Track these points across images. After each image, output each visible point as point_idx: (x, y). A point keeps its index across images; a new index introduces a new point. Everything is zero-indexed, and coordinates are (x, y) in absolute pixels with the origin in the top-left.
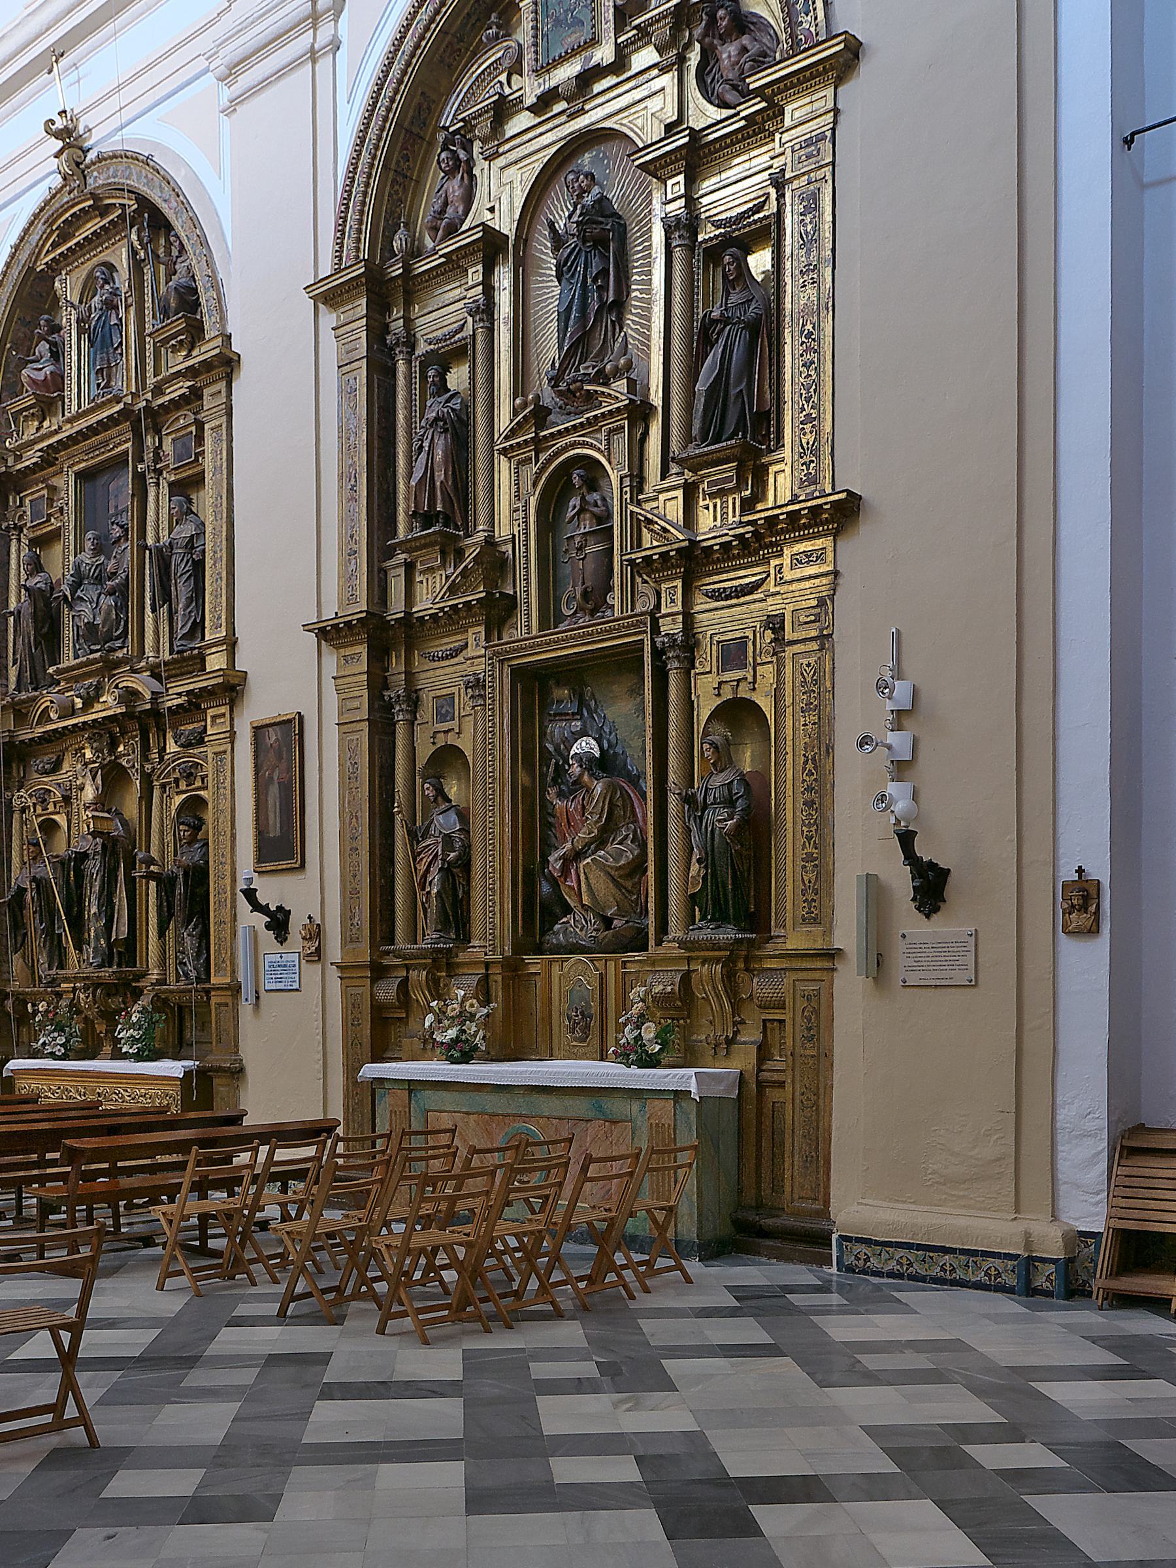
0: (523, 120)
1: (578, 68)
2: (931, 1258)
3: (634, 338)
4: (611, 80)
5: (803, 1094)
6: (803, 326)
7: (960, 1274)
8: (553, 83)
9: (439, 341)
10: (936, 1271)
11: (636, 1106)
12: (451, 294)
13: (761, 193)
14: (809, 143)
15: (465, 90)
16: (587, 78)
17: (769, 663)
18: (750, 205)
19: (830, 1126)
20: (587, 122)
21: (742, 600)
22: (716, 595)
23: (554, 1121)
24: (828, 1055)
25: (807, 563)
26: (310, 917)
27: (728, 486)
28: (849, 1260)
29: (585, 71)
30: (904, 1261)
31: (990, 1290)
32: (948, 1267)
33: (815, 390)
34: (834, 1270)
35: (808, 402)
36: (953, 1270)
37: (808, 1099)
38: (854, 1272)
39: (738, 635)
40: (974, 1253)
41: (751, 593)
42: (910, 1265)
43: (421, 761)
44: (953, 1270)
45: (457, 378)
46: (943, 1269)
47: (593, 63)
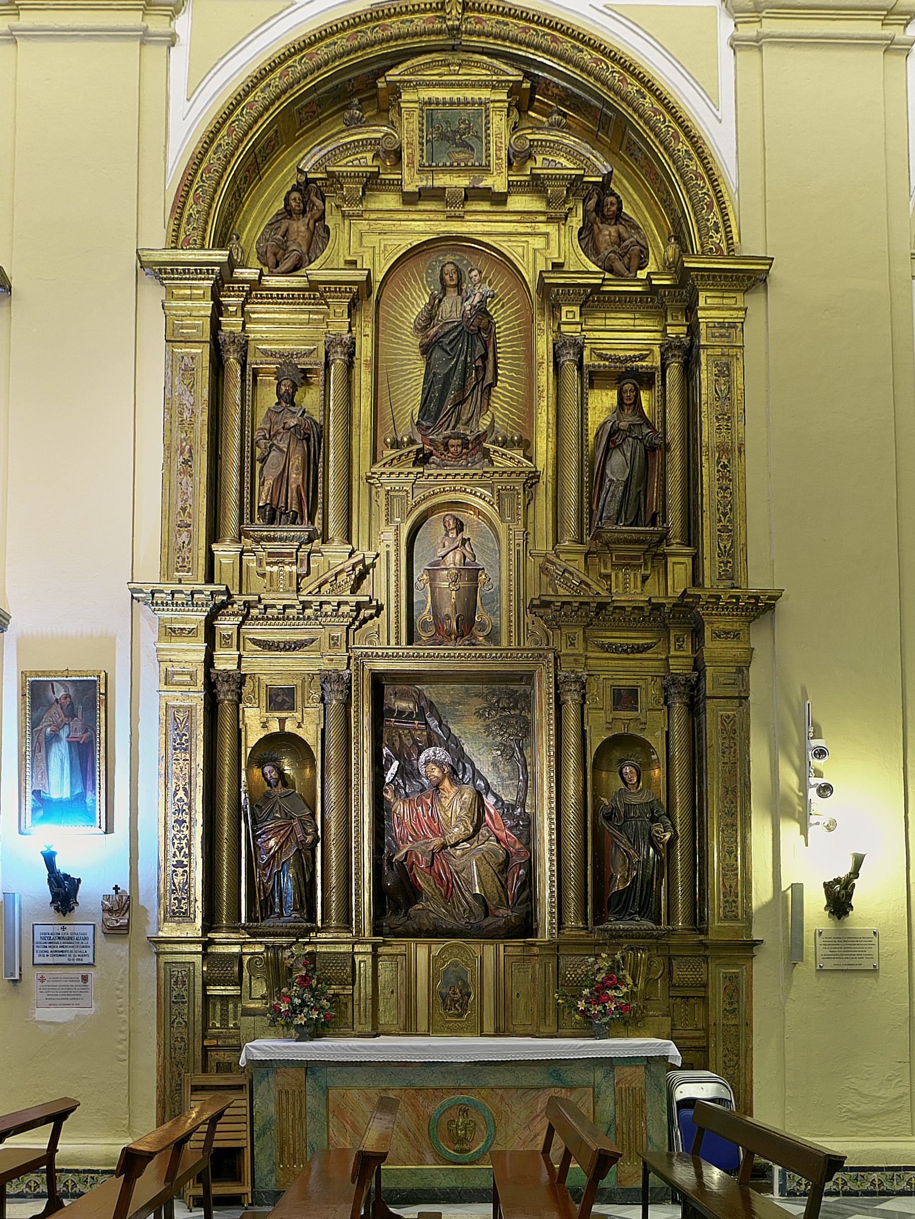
0: (390, 201)
1: (467, 182)
2: (863, 1177)
3: (500, 419)
4: (486, 206)
5: (725, 1056)
6: (719, 458)
7: (887, 1186)
8: (437, 184)
9: (618, 359)
10: (867, 1186)
11: (599, 1075)
12: (619, 322)
13: (645, 347)
14: (722, 325)
15: (330, 148)
16: (472, 194)
17: (660, 710)
18: (637, 353)
19: (752, 1080)
20: (464, 229)
21: (631, 656)
22: (603, 648)
23: (499, 1091)
24: (749, 1025)
25: (726, 638)
26: (116, 888)
27: (288, 560)
28: (790, 1186)
29: (474, 188)
30: (840, 1181)
31: (911, 1195)
32: (877, 1182)
33: (731, 509)
34: (776, 1195)
35: (725, 516)
36: (881, 1184)
37: (730, 1060)
38: (795, 1195)
39: (631, 683)
40: (898, 1169)
41: (641, 652)
42: (845, 1183)
43: (594, 743)
44: (881, 1184)
45: (310, 399)
46: (872, 1184)
47: (482, 185)
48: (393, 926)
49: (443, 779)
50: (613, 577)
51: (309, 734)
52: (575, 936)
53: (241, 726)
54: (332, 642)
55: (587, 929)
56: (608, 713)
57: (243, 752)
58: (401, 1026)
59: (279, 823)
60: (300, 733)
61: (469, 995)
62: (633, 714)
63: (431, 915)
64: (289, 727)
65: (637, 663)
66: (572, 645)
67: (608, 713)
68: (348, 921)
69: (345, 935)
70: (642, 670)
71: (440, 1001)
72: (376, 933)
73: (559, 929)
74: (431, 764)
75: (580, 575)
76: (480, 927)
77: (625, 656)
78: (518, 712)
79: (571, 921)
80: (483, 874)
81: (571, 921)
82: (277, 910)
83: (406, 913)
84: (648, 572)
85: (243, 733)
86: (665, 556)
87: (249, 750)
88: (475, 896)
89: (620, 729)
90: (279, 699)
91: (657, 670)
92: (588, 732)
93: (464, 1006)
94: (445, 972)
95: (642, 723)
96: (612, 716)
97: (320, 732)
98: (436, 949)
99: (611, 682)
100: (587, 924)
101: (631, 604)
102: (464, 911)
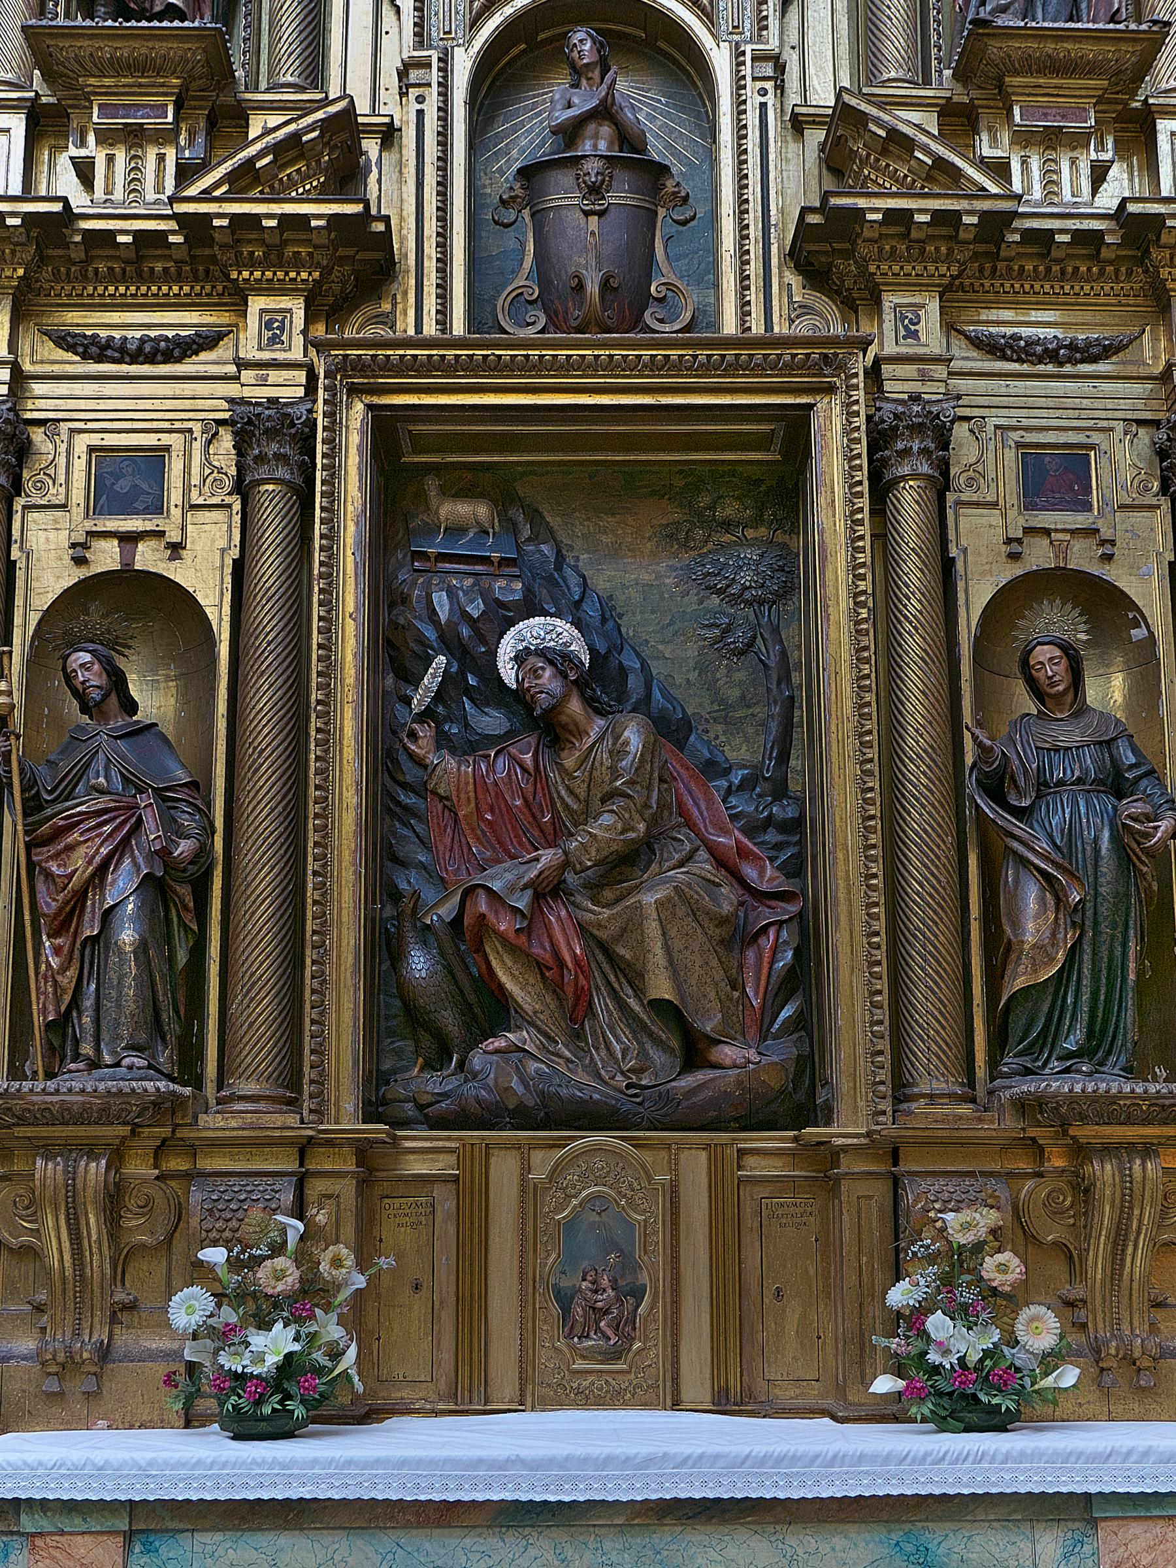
21: (1068, 369)
43: (977, 594)
48: (425, 1099)
49: (565, 697)
50: (1016, 166)
51: (203, 577)
52: (945, 1119)
53: (15, 554)
54: (267, 334)
55: (973, 1101)
56: (1012, 513)
57: (18, 620)
58: (442, 1386)
59: (103, 802)
60: (181, 574)
61: (638, 1293)
62: (1079, 520)
63: (533, 1066)
64: (148, 557)
65: (1086, 387)
66: (911, 326)
67: (1012, 513)
68: (295, 1084)
69: (279, 1120)
70: (1098, 404)
71: (555, 1309)
72: (372, 1111)
73: (897, 1100)
74: (532, 660)
75: (934, 146)
76: (667, 1098)
77: (1050, 368)
78: (763, 531)
79: (932, 1077)
80: (677, 945)
81: (932, 1077)
82: (87, 1049)
83: (461, 1065)
84: (1108, 156)
85: (20, 574)
86: (838, 1180)
87: (34, 618)
88: (659, 1006)
89: (1039, 556)
90: (123, 486)
91: (1140, 404)
92: (959, 565)
93: (625, 1327)
94: (570, 1225)
95: (1103, 542)
96: (1021, 522)
97: (229, 570)
98: (542, 1163)
99: (1015, 436)
100: (971, 1084)
101: (1070, 224)
102: (624, 1052)
